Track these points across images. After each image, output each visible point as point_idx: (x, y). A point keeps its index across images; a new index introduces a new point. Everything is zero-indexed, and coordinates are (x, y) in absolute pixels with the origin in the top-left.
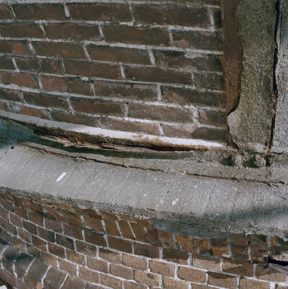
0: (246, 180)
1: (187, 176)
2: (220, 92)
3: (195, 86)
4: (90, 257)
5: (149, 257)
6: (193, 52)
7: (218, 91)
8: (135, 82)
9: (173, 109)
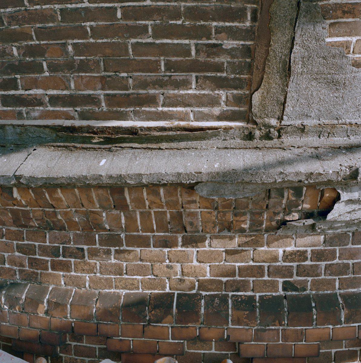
0: (266, 148)
1: (218, 150)
2: (246, 76)
3: (227, 72)
4: (103, 262)
5: (168, 248)
6: (229, 44)
7: (244, 76)
8: (172, 74)
9: (205, 95)
